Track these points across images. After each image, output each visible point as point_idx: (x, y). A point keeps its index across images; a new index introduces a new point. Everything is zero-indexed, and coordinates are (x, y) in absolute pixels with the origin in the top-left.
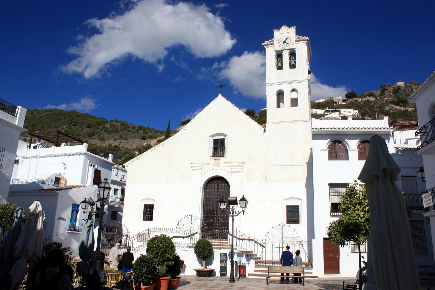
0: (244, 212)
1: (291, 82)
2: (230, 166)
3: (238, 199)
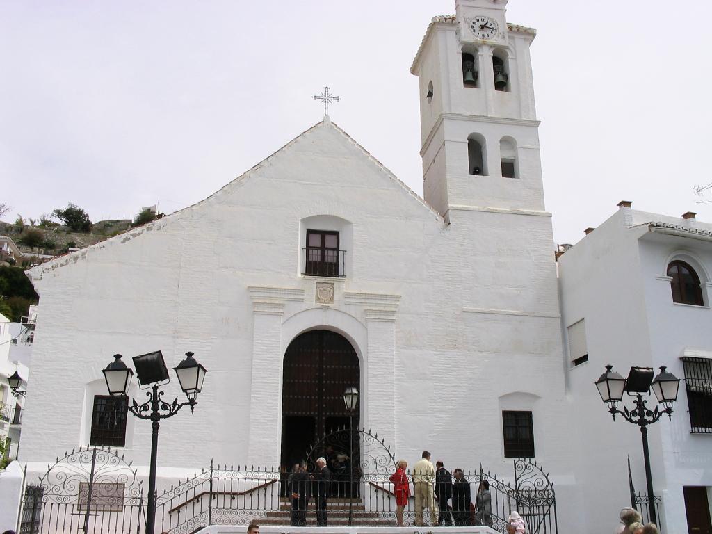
0: (192, 402)
1: (506, 121)
3: (172, 360)
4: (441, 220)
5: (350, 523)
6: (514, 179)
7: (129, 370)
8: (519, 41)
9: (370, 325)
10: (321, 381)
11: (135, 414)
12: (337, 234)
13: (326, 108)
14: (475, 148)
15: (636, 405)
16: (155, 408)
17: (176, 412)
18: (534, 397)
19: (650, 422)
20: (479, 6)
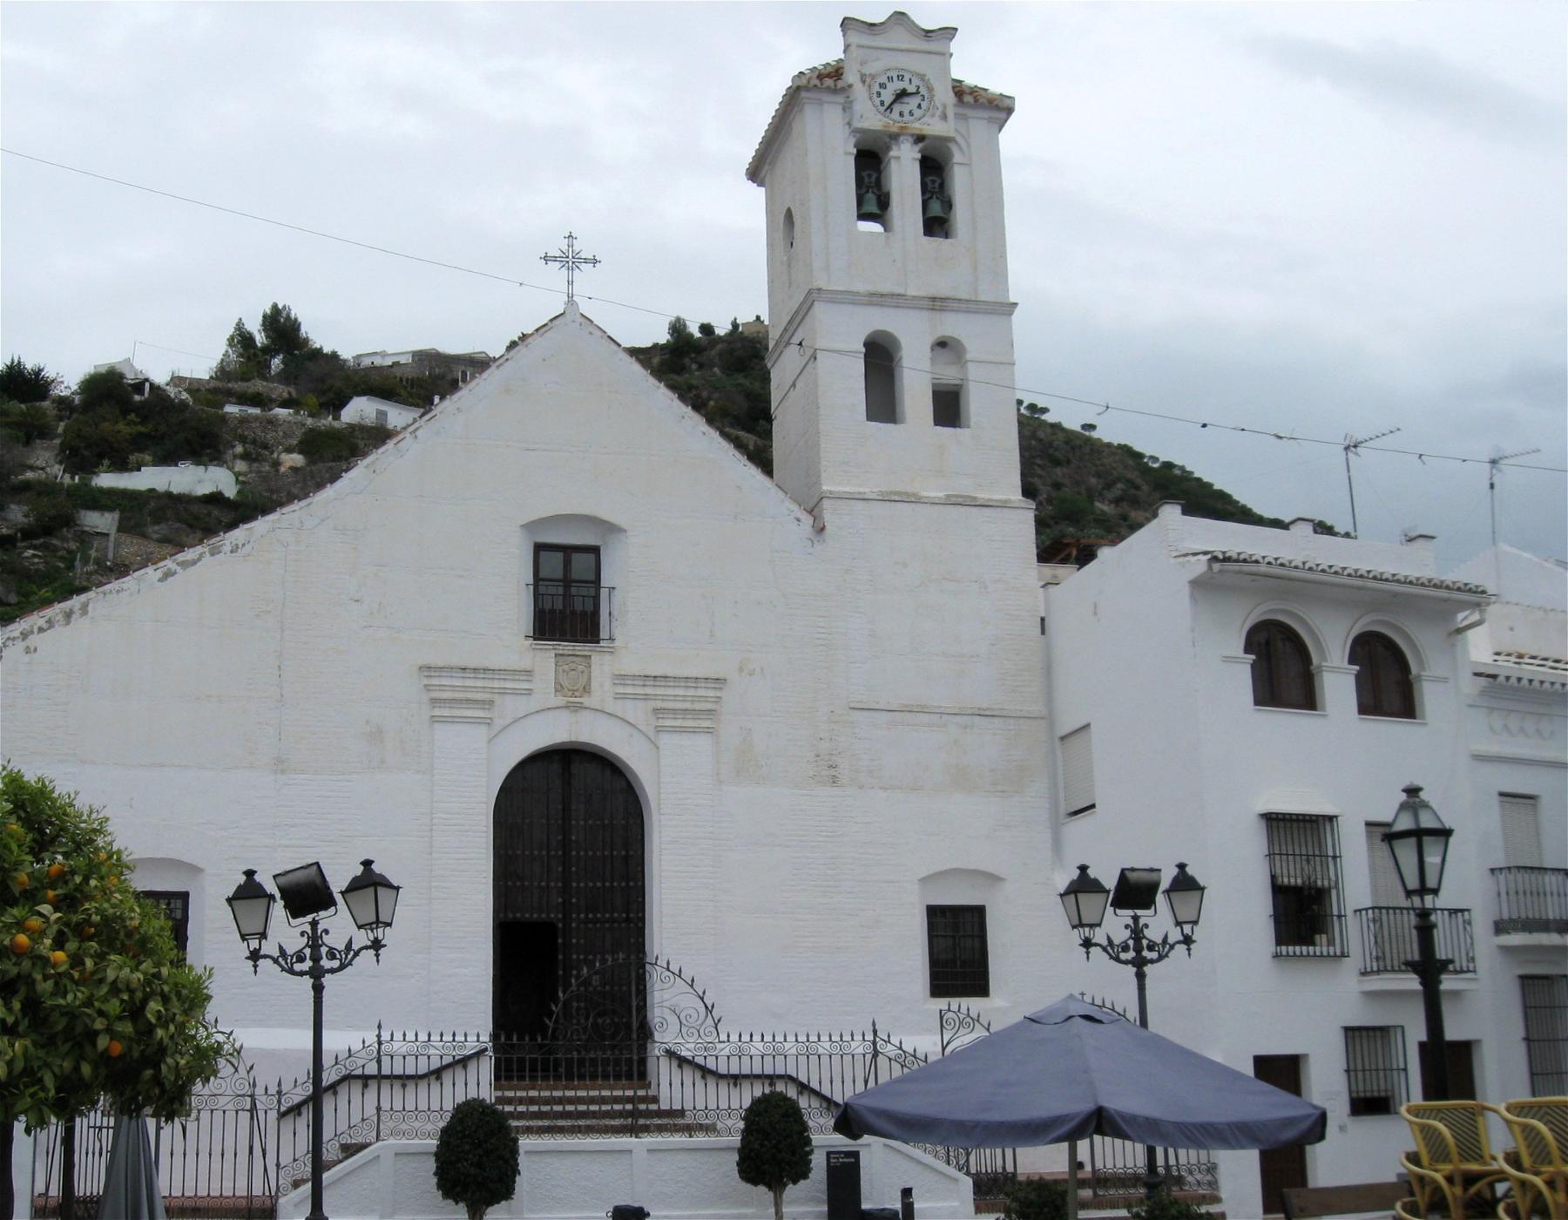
0: (377, 945)
2: (646, 697)
3: (338, 882)
4: (807, 520)
5: (634, 1130)
6: (958, 430)
7: (272, 897)
8: (978, 125)
9: (665, 740)
10: (571, 854)
11: (283, 969)
12: (595, 550)
13: (570, 283)
14: (880, 358)
15: (1128, 933)
16: (316, 959)
17: (350, 964)
18: (994, 879)
19: (1152, 961)
20: (895, 45)
